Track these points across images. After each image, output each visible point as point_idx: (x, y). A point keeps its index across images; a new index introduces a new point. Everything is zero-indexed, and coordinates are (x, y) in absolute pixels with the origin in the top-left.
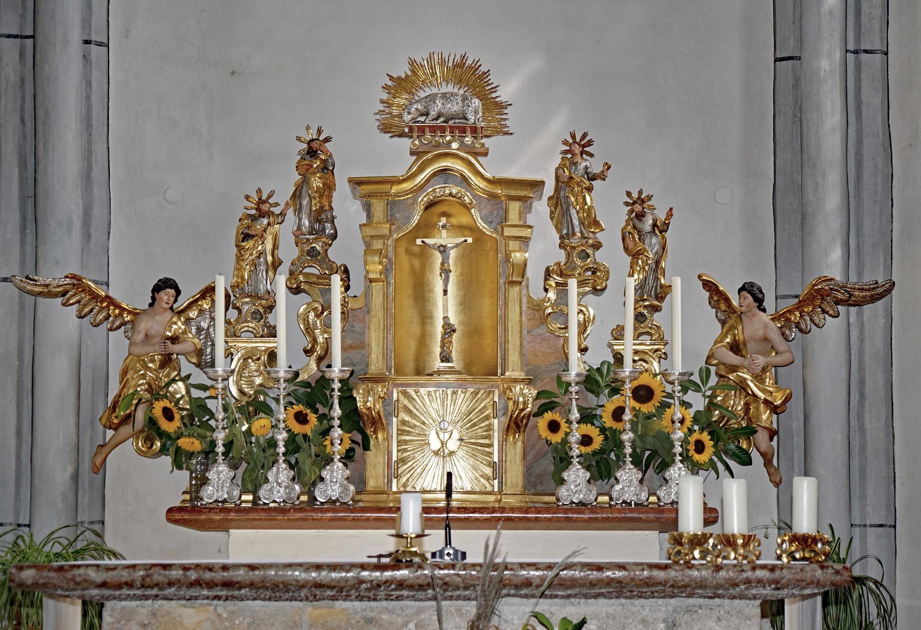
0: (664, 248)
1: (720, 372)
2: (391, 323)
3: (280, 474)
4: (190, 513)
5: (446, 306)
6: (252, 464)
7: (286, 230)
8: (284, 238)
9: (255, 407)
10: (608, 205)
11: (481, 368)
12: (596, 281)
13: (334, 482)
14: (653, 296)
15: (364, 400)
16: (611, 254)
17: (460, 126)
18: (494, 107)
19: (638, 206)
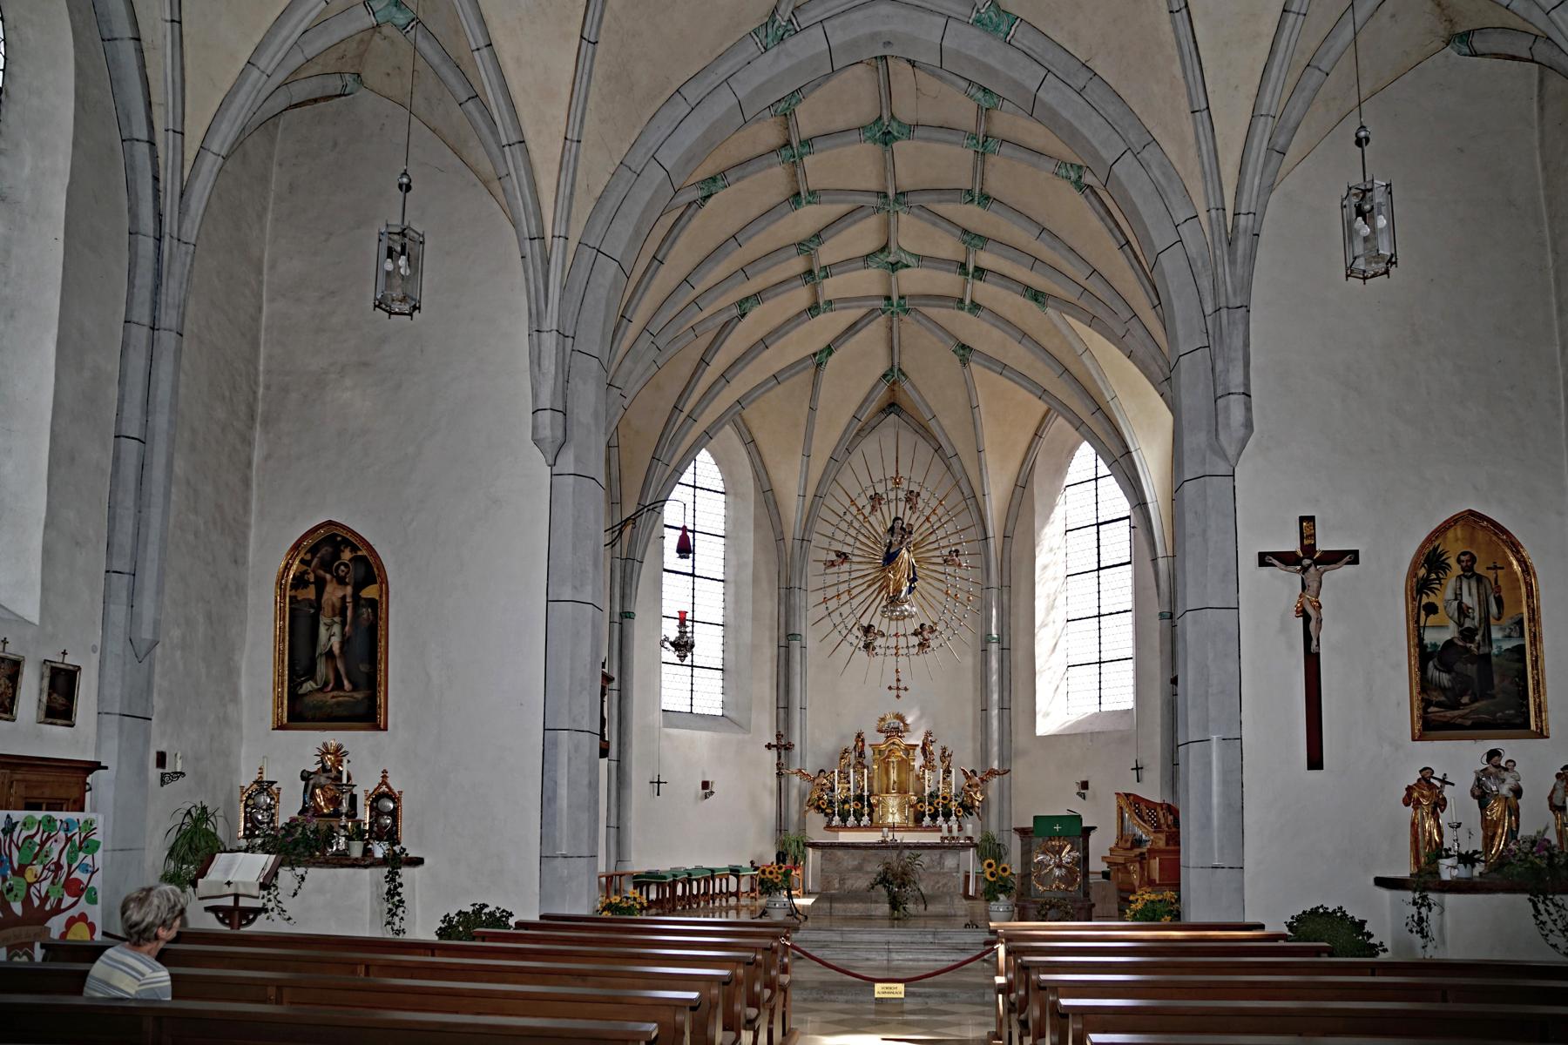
0: (123, 913)
1: (963, 791)
2: (880, 780)
3: (852, 818)
4: (829, 827)
5: (894, 776)
6: (844, 817)
7: (852, 756)
8: (852, 757)
9: (845, 801)
10: (935, 749)
11: (902, 791)
12: (933, 769)
13: (865, 820)
14: (948, 772)
15: (873, 801)
16: (937, 762)
17: (897, 730)
18: (906, 725)
19: (944, 750)
